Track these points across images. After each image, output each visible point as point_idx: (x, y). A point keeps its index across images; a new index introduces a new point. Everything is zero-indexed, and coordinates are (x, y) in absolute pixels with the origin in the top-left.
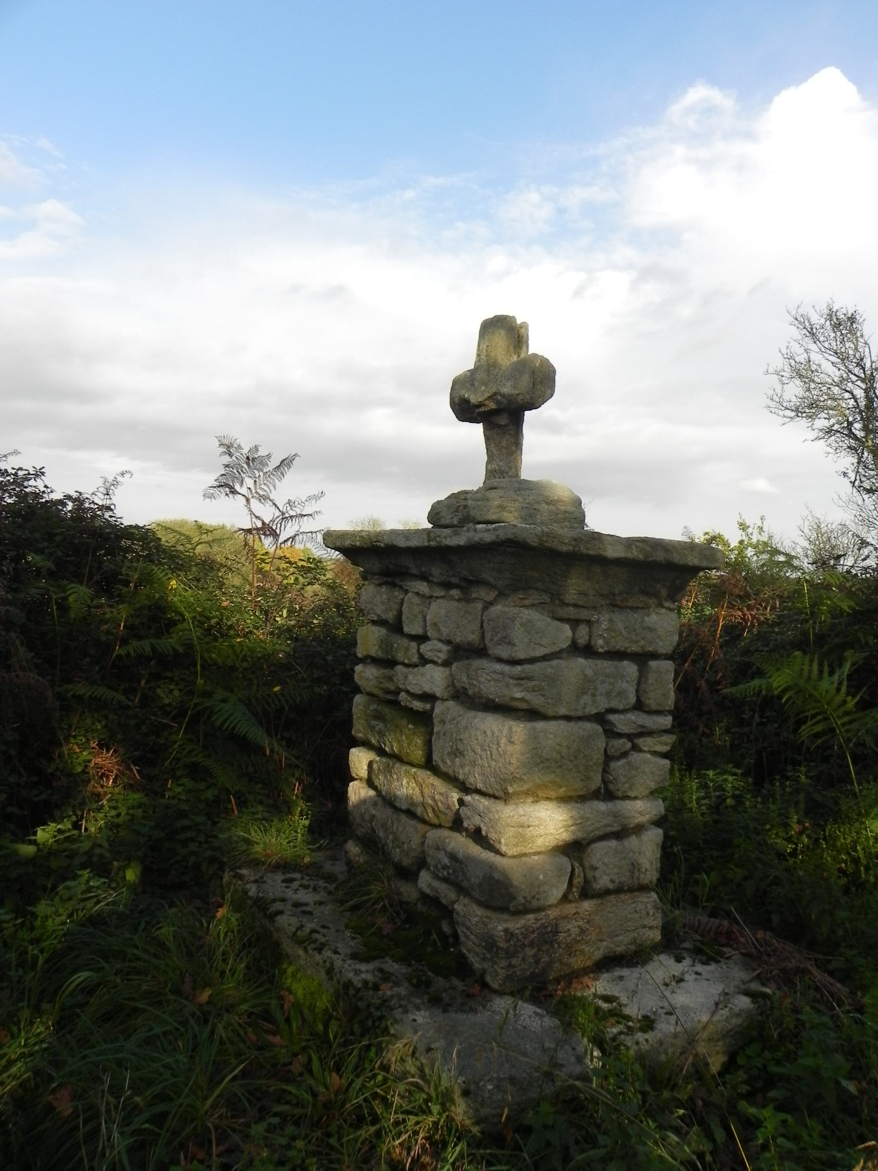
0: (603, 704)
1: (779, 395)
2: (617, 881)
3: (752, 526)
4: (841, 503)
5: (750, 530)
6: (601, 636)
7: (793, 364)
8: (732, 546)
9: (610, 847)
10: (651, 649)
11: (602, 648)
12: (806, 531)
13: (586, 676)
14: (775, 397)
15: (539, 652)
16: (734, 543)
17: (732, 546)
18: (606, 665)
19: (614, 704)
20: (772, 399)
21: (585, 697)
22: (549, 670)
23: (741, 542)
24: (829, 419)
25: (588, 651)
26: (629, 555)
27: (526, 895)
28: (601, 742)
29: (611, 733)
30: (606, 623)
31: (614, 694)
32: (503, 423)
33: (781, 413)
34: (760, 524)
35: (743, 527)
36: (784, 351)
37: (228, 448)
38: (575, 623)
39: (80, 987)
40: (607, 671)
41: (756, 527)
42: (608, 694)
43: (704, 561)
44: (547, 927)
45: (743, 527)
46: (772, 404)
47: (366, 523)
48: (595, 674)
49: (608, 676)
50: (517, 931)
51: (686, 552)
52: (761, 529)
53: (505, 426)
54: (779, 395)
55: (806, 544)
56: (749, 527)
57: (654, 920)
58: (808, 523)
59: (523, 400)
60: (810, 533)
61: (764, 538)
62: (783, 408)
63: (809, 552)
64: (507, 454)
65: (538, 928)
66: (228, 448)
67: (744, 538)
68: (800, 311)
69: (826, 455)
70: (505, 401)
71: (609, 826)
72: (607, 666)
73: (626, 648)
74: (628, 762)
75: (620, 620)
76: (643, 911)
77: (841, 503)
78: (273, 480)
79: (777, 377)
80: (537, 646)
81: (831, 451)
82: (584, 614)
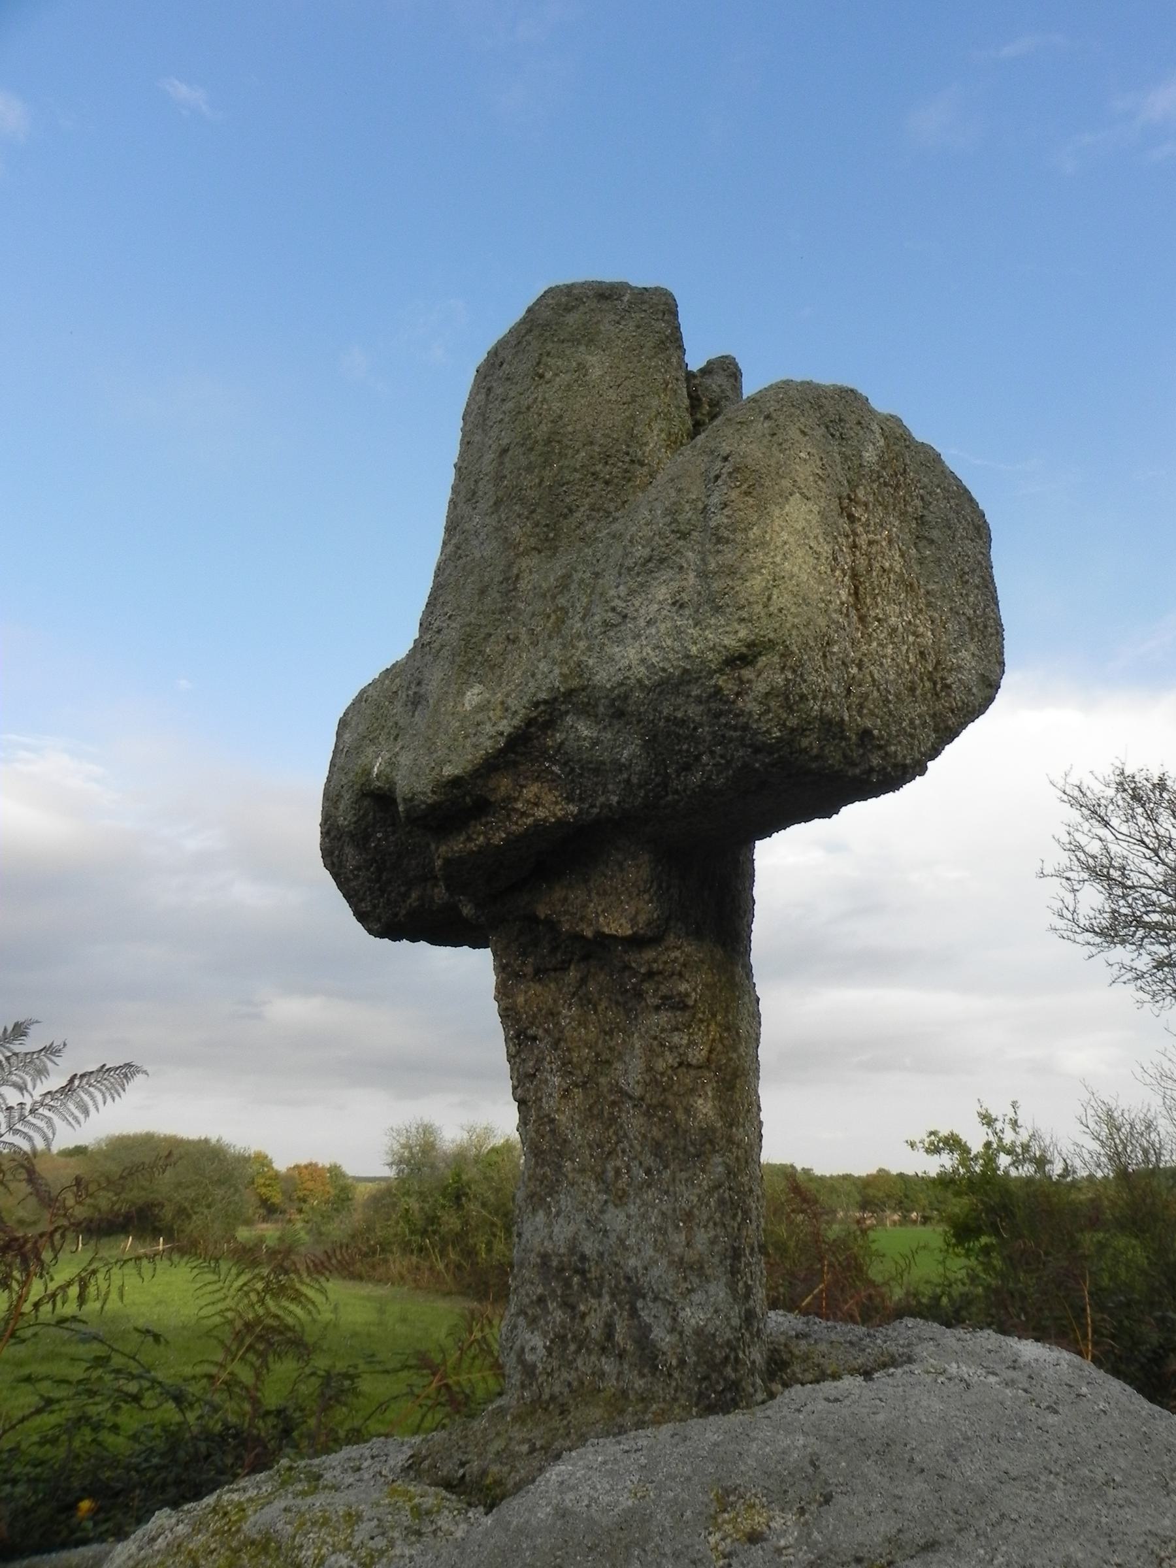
1: (1071, 909)
3: (1001, 1118)
4: (1149, 1080)
5: (998, 1126)
7: (1082, 857)
8: (974, 1152)
12: (1092, 1125)
14: (1065, 912)
16: (976, 1147)
17: (974, 1152)
20: (1062, 916)
23: (988, 1145)
24: (1168, 944)
32: (618, 926)
33: (1079, 938)
34: (1011, 1115)
35: (988, 1120)
36: (1065, 839)
41: (1007, 1121)
45: (988, 1120)
46: (1061, 924)
47: (413, 1130)
52: (1015, 1124)
53: (636, 942)
54: (1071, 909)
55: (1095, 1146)
56: (996, 1120)
58: (1093, 1112)
59: (788, 699)
60: (1097, 1128)
61: (1024, 1137)
62: (1079, 930)
63: (1103, 1159)
64: (657, 1148)
67: (992, 1138)
68: (1069, 780)
69: (1139, 1005)
70: (630, 750)
77: (1149, 1080)
78: (49, 1122)
79: (1058, 880)
81: (1148, 997)
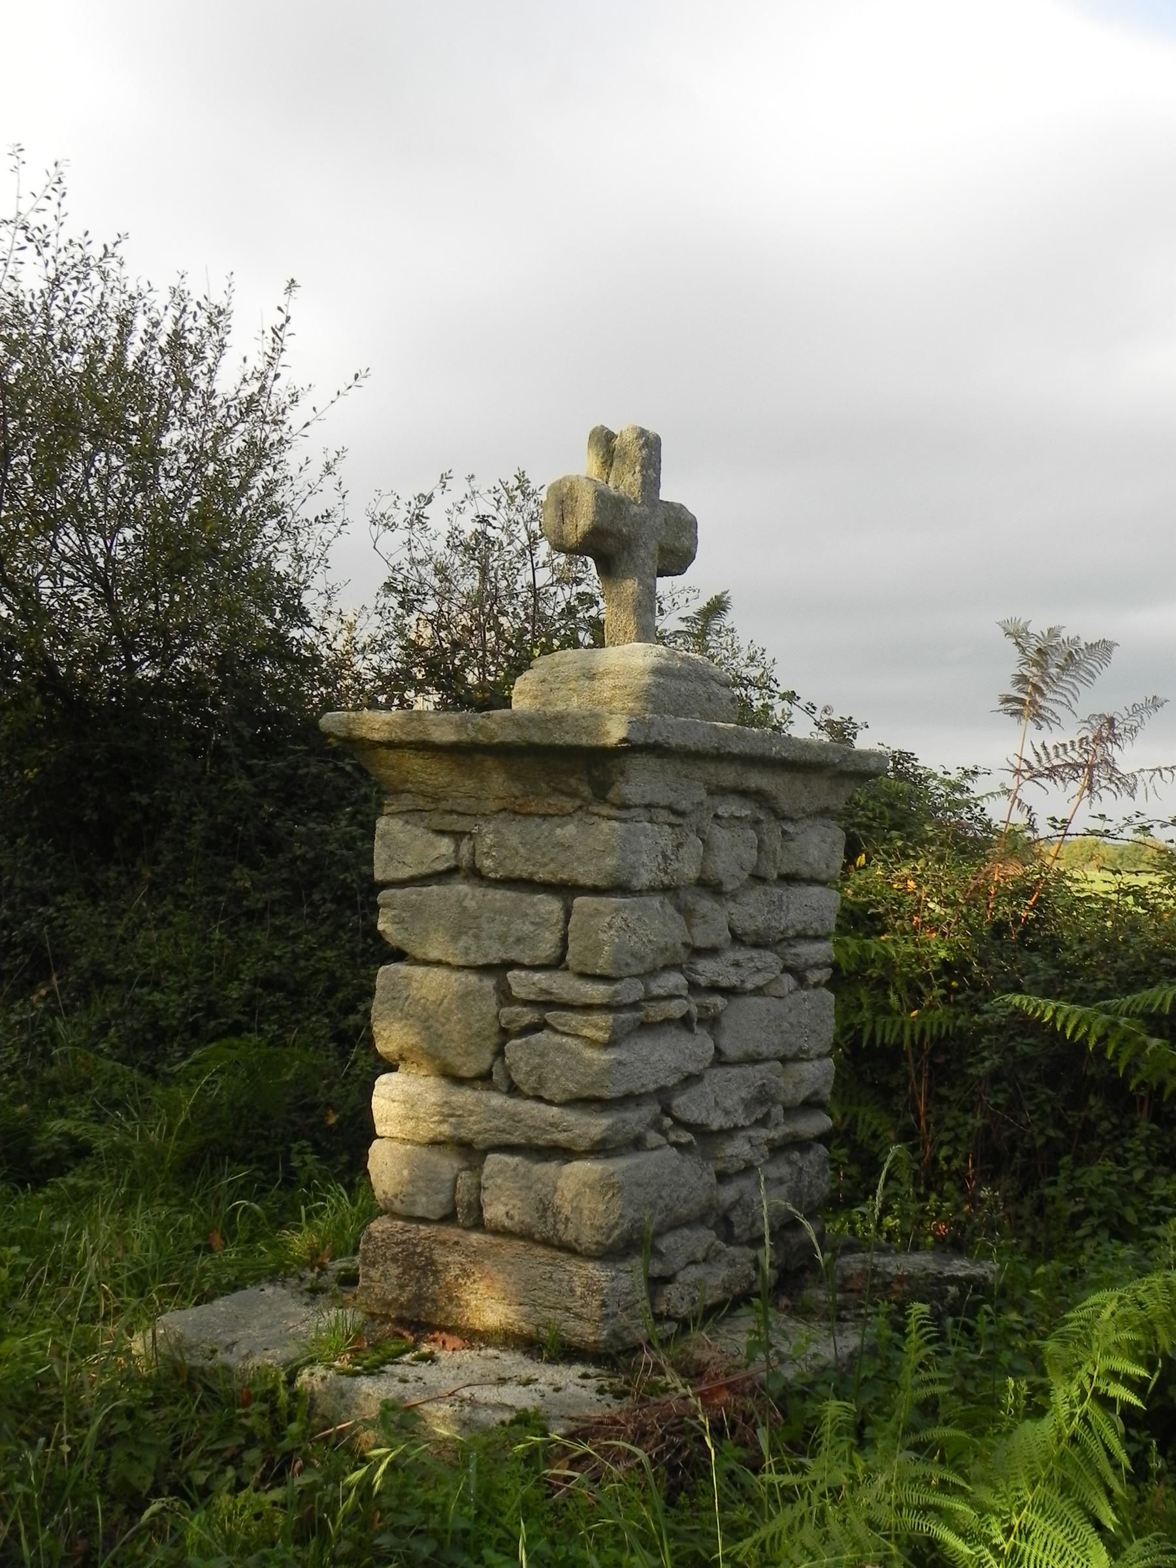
0: (495, 953)
2: (516, 1218)
6: (487, 855)
9: (507, 1164)
10: (565, 877)
11: (496, 871)
13: (465, 909)
15: (405, 873)
18: (497, 897)
19: (514, 955)
21: (464, 937)
22: (414, 897)
25: (476, 875)
26: (464, 737)
27: (386, 1189)
28: (490, 1005)
29: (505, 996)
30: (491, 836)
31: (511, 940)
37: (1018, 635)
38: (457, 836)
39: (929, 1336)
40: (498, 904)
42: (502, 938)
43: (583, 736)
44: (416, 1245)
48: (480, 908)
49: (499, 912)
50: (377, 1234)
51: (550, 725)
57: (582, 1306)
65: (404, 1242)
66: (1018, 635)
71: (503, 1131)
72: (501, 897)
73: (532, 874)
74: (527, 1042)
75: (513, 833)
76: (564, 1284)
80: (400, 866)
82: (461, 824)
